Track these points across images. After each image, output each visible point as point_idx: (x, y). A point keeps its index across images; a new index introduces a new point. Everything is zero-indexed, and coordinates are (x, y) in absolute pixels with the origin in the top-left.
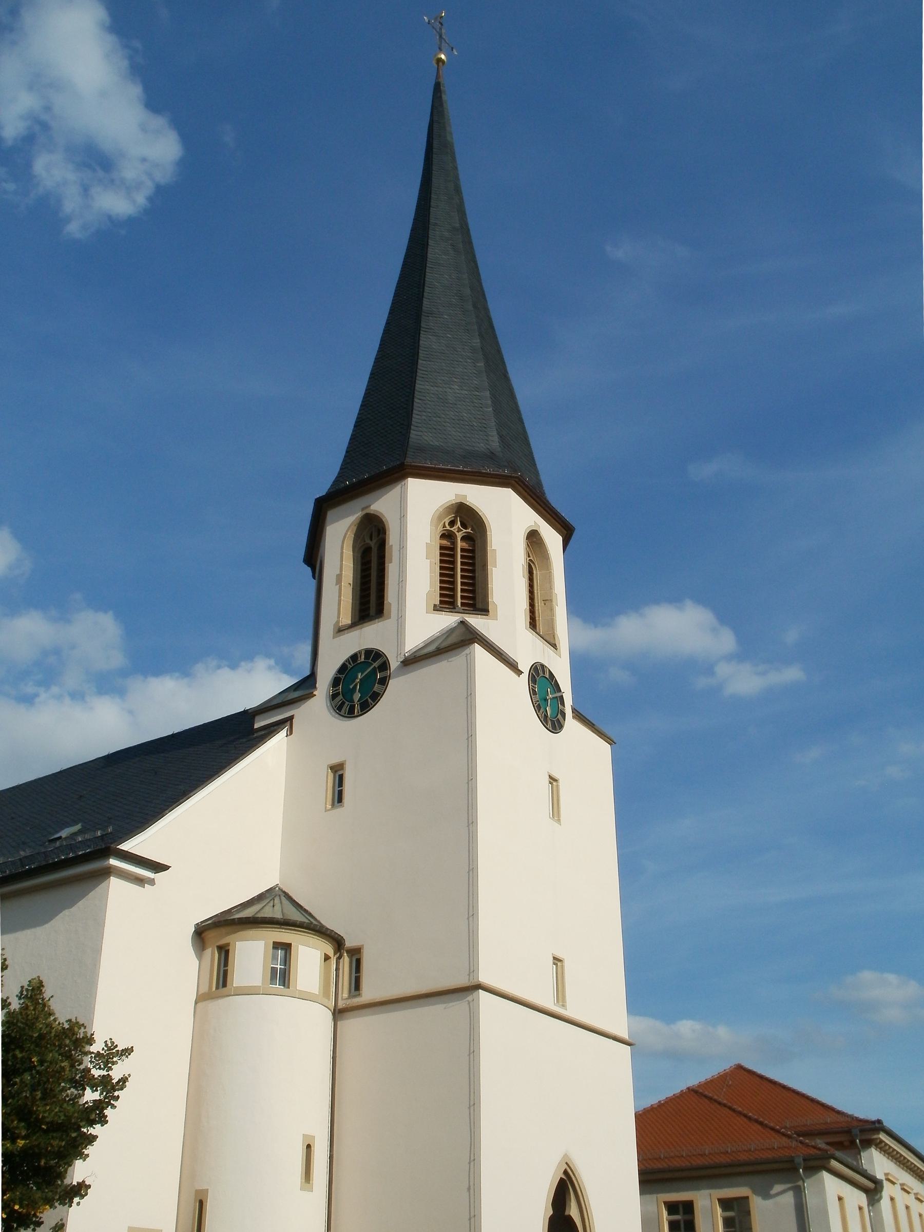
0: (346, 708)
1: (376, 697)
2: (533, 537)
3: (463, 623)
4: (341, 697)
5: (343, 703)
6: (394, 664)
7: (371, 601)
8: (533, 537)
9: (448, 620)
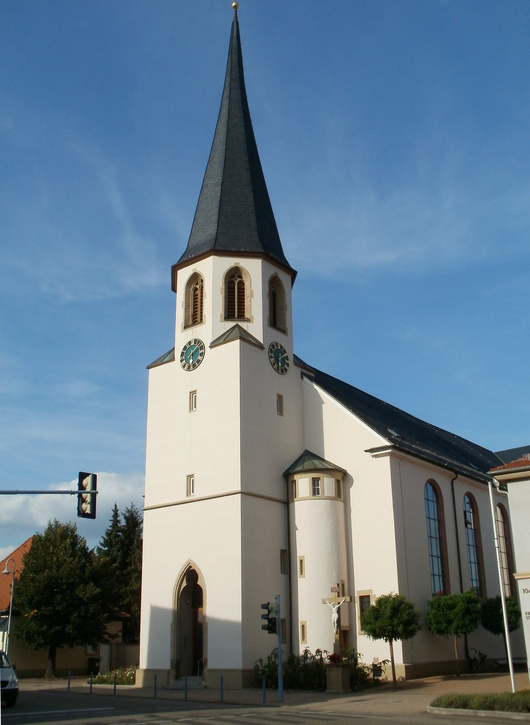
0: (186, 367)
1: (199, 362)
2: (432, 483)
3: (237, 325)
4: (184, 361)
5: (185, 364)
6: (207, 344)
7: (195, 317)
8: (432, 483)
9: (231, 324)
